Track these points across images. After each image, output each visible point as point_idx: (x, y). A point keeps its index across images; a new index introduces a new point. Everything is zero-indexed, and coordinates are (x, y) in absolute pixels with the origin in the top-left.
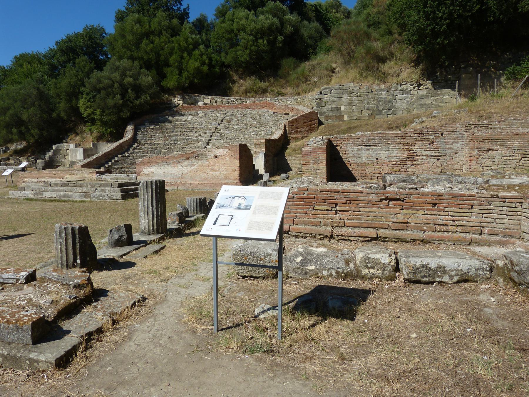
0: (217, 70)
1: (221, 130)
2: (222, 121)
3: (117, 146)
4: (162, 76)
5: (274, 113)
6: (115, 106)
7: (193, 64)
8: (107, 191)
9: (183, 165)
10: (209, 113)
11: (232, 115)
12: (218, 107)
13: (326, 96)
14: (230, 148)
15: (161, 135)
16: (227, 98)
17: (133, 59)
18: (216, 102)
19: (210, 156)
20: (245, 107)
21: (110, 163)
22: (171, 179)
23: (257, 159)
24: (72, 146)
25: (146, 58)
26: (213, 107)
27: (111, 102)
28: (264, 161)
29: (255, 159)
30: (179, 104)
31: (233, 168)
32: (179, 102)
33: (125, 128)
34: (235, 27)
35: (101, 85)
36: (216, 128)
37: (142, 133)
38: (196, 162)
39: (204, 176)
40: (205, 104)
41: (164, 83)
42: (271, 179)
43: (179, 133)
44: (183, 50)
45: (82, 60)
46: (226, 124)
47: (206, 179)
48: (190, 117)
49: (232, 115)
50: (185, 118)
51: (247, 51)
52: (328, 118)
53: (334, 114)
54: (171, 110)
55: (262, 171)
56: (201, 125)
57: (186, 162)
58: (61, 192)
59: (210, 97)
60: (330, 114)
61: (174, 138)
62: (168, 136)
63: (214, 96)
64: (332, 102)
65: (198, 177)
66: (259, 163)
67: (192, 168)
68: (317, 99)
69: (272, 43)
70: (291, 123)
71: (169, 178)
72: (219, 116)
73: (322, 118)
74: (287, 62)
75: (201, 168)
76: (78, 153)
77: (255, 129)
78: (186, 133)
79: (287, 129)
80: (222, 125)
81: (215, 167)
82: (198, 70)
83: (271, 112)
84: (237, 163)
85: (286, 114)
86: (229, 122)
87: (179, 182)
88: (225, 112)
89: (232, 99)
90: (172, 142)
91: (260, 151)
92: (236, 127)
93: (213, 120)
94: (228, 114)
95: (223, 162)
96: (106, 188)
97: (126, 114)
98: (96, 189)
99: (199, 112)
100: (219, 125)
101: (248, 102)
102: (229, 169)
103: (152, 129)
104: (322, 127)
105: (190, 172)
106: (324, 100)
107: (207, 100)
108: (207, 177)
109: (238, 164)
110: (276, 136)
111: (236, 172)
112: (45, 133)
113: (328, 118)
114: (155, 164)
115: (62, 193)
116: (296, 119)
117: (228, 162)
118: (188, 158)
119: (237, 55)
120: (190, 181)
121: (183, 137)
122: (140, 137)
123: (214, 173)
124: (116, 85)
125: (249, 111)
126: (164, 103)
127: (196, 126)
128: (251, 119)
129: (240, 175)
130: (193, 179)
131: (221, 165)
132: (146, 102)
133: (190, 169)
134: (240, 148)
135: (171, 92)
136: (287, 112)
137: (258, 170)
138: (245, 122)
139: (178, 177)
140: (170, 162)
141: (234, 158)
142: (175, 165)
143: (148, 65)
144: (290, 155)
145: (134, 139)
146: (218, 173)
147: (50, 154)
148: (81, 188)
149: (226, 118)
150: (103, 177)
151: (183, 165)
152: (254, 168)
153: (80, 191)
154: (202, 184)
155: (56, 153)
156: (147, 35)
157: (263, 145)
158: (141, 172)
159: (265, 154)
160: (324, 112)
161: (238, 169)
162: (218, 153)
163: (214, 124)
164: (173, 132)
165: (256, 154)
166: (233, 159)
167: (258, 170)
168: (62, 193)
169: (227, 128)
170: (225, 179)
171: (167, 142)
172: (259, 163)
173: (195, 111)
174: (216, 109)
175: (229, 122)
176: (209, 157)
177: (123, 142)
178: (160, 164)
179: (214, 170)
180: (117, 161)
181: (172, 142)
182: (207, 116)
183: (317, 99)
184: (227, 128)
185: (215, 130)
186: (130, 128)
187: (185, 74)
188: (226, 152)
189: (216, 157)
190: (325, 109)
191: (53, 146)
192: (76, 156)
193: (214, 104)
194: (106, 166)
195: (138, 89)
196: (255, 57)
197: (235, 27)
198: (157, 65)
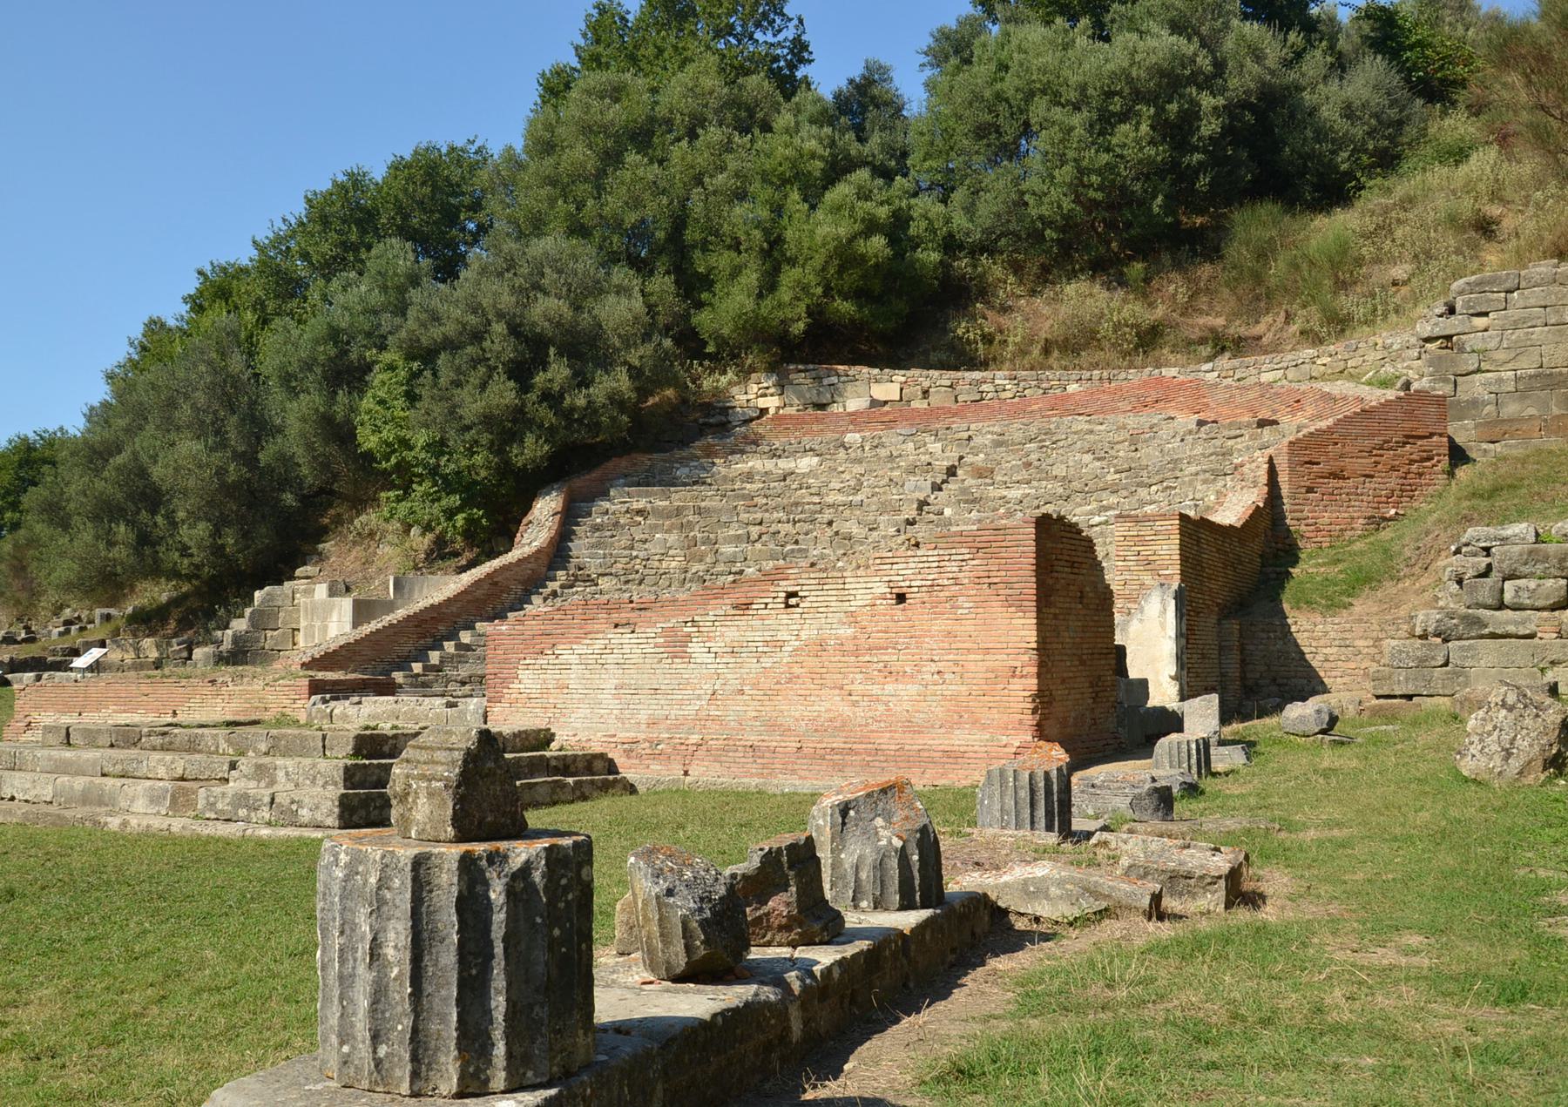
0: (930, 257)
1: (948, 512)
2: (951, 472)
3: (477, 584)
4: (694, 286)
5: (1201, 423)
6: (487, 420)
7: (821, 228)
8: (281, 774)
9: (717, 646)
10: (892, 440)
11: (998, 444)
12: (933, 413)
13: (1480, 322)
14: (983, 544)
15: (672, 538)
16: (977, 375)
17: (578, 230)
18: (926, 393)
19: (868, 590)
20: (1064, 407)
21: (434, 657)
22: (652, 723)
23: (1134, 626)
24: (321, 590)
25: (631, 218)
26: (912, 417)
27: (472, 405)
28: (1171, 630)
29: (1126, 623)
30: (764, 411)
31: (1001, 661)
32: (762, 403)
33: (528, 508)
34: (1010, 84)
35: (436, 333)
36: (922, 504)
37: (597, 528)
38: (790, 629)
39: (830, 705)
40: (875, 403)
41: (703, 320)
42: (1228, 731)
43: (755, 531)
44: (785, 182)
45: (395, 254)
46: (970, 482)
47: (843, 726)
48: (806, 463)
49: (998, 444)
50: (785, 464)
51: (1066, 173)
52: (1496, 430)
53: (1532, 411)
54: (714, 425)
55: (1163, 693)
56: (856, 490)
57: (733, 632)
58: (77, 774)
59: (899, 376)
60: (1511, 409)
61: (728, 549)
62: (706, 541)
63: (915, 372)
64: (1519, 350)
65: (797, 710)
66: (1150, 642)
67: (767, 662)
68: (1428, 340)
69: (1177, 132)
70: (1307, 450)
71: (643, 716)
72: (939, 453)
73: (1463, 432)
74: (1254, 224)
75: (812, 662)
76: (335, 617)
77: (1113, 499)
78: (786, 528)
79: (1283, 478)
80: (952, 486)
81: (890, 657)
82: (845, 256)
83: (1187, 421)
84: (1024, 630)
85: (1262, 424)
86: (981, 473)
87: (695, 738)
88: (966, 435)
89: (1001, 377)
90: (720, 568)
91: (1147, 579)
92: (1015, 493)
93: (912, 470)
94: (978, 440)
95: (940, 625)
96: (280, 762)
97: (531, 450)
98: (233, 766)
99: (850, 438)
100: (937, 488)
101: (1073, 388)
102: (977, 665)
103: (639, 512)
104: (1463, 473)
105: (755, 686)
106: (1472, 341)
107: (888, 386)
108: (847, 711)
109: (1031, 636)
110: (1232, 511)
111: (1017, 684)
112: (229, 540)
113: (1496, 430)
114: (578, 639)
115: (79, 783)
116: (1329, 431)
117: (968, 627)
118: (747, 606)
119: (1023, 193)
120: (753, 738)
121: (772, 546)
122: (580, 548)
123: (890, 688)
124: (499, 328)
125: (1081, 424)
126: (708, 408)
127: (830, 499)
128: (1088, 458)
129: (1044, 700)
130: (772, 726)
131: (929, 643)
132: (616, 400)
133: (752, 666)
134: (1038, 540)
135: (727, 355)
136: (1265, 414)
137: (1143, 683)
138: (1060, 470)
139: (689, 711)
140: (653, 628)
141: (1008, 602)
142: (677, 646)
143: (637, 251)
144: (1333, 601)
145: (557, 553)
146: (913, 689)
147: (240, 625)
148: (168, 757)
149: (969, 459)
150: (339, 707)
151: (717, 646)
152: (1122, 669)
153: (162, 772)
154: (819, 756)
155: (262, 621)
156: (642, 136)
157: (1168, 549)
158: (506, 682)
159: (1179, 596)
160: (1475, 403)
161: (1028, 663)
162: (908, 572)
163: (918, 487)
164: (727, 524)
165: (1129, 599)
166: (996, 607)
167: (1143, 683)
168: (79, 783)
169: (975, 501)
170: (949, 726)
171: (696, 567)
172: (1150, 642)
173: (830, 436)
174: (926, 423)
175: (981, 473)
176: (861, 599)
177: (504, 568)
178: (599, 644)
179: (889, 673)
180: (468, 648)
181: (720, 568)
182: (883, 452)
183: (1428, 340)
184: (975, 501)
185: (920, 509)
186: (546, 508)
187: (789, 276)
188: (960, 565)
189: (901, 598)
190: (1476, 387)
191: (257, 594)
192: (325, 629)
193: (918, 404)
194: (417, 667)
195: (586, 350)
196: (1099, 196)
197: (1010, 84)
198: (672, 250)
